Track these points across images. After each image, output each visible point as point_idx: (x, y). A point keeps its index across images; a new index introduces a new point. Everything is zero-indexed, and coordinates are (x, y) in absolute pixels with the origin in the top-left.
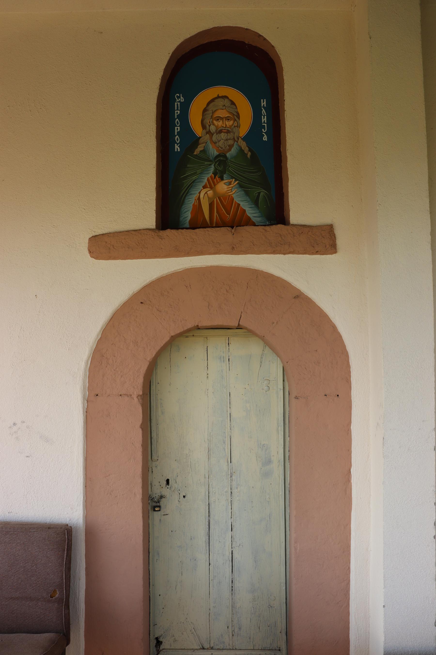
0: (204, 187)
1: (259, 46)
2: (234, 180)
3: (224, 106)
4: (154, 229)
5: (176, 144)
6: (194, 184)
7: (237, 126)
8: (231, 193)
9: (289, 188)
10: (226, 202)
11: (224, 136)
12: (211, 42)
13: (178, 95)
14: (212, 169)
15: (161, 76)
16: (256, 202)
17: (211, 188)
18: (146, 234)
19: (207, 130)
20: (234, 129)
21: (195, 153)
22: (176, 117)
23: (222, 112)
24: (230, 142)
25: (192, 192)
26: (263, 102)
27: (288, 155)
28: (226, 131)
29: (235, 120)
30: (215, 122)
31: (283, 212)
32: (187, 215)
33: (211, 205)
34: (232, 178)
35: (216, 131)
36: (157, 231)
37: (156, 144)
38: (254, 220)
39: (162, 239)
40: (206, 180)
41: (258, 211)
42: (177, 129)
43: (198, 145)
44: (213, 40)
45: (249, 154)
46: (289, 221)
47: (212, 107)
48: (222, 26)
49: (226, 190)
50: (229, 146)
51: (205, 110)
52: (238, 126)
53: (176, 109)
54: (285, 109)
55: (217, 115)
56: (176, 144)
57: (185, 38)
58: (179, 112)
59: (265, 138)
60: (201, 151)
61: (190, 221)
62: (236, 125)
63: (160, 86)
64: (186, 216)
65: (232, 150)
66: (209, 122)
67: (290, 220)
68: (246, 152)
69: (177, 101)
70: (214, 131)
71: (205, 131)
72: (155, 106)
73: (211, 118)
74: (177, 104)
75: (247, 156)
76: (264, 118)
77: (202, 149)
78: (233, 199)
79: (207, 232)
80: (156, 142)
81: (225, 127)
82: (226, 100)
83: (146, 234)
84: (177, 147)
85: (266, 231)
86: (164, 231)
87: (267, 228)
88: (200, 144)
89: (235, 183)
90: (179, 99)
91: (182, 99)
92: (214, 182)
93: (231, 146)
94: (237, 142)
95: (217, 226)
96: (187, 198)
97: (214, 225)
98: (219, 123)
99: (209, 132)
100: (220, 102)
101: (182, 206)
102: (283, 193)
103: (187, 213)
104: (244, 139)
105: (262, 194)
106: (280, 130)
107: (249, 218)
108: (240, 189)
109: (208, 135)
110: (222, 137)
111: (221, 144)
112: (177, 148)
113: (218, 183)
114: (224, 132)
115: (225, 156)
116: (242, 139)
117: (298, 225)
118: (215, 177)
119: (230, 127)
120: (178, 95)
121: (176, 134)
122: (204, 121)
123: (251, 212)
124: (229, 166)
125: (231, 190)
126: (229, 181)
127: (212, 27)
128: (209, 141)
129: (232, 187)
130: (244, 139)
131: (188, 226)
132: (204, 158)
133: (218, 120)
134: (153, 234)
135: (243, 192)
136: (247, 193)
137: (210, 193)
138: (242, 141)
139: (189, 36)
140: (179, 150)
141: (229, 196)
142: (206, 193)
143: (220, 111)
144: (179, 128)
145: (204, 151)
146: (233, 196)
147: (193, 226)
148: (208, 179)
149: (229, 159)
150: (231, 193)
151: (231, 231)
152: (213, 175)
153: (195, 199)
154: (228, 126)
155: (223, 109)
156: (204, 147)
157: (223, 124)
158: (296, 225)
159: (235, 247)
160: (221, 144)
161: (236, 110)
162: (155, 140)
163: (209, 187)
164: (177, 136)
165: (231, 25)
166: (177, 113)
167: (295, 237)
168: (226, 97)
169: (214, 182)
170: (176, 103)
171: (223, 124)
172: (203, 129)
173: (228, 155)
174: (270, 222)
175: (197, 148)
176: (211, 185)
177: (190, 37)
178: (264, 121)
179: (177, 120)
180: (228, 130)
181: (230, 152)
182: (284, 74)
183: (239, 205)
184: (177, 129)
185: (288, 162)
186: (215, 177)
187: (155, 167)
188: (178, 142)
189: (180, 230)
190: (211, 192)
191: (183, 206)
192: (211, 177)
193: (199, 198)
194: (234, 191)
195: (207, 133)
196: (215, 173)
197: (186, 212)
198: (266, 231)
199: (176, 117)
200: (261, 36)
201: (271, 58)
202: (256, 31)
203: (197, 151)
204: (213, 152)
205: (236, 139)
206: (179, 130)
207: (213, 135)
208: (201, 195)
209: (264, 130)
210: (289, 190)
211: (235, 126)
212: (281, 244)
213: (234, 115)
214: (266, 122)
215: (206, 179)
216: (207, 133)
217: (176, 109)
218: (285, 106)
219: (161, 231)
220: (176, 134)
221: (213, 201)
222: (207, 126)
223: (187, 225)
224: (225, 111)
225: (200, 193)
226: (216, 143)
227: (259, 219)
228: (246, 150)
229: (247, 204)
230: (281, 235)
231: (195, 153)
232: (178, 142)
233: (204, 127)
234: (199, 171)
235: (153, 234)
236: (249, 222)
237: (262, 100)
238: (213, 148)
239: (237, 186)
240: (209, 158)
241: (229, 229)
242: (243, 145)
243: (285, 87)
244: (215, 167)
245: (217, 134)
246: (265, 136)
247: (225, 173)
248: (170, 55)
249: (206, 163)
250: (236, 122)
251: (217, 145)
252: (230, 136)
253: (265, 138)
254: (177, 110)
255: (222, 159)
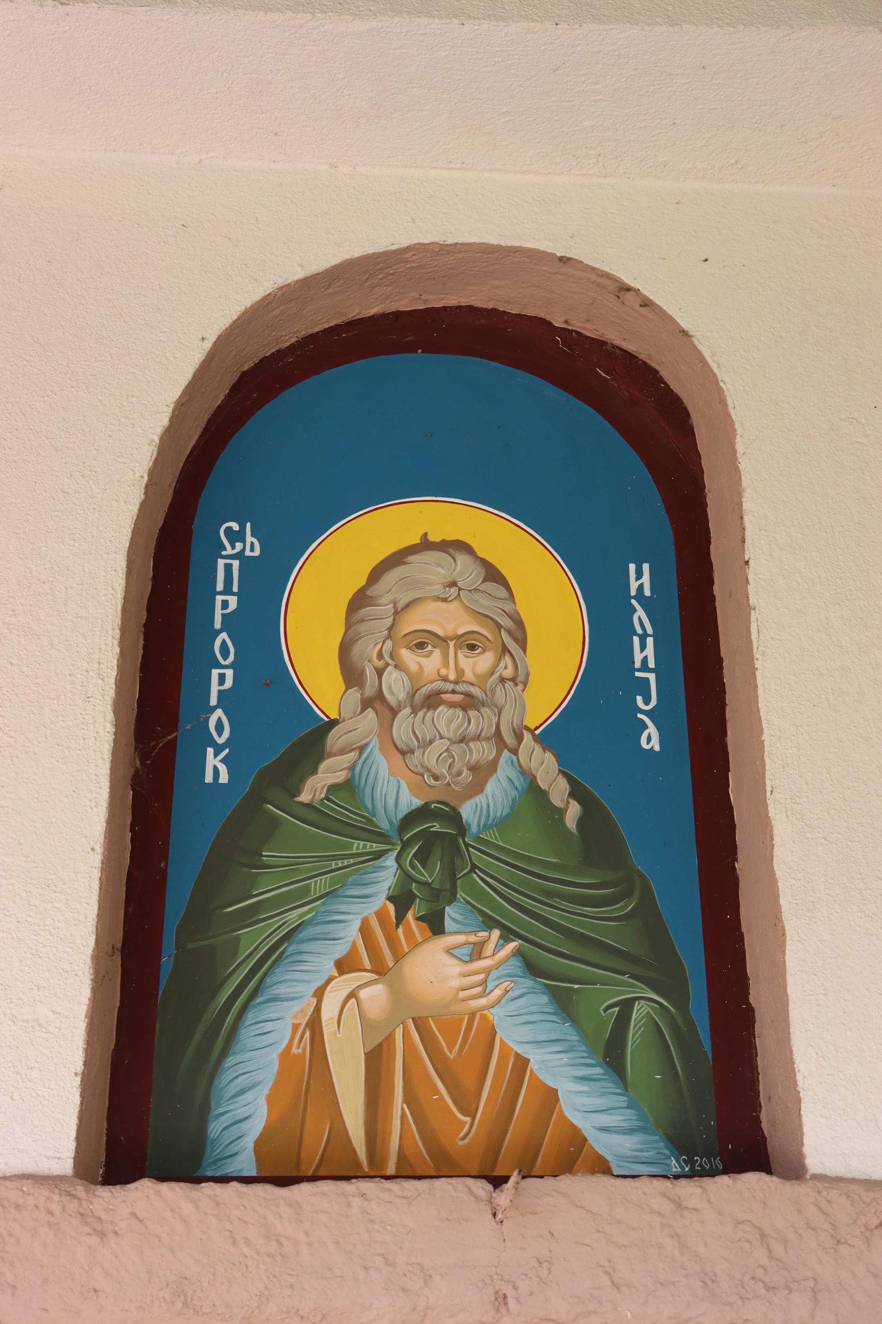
0: (344, 966)
1: (614, 336)
2: (496, 933)
3: (454, 584)
4: (61, 1178)
5: (210, 751)
6: (293, 948)
7: (513, 680)
8: (483, 1001)
9: (790, 980)
10: (455, 1046)
11: (450, 721)
12: (398, 314)
13: (235, 526)
14: (387, 874)
15: (159, 431)
16: (612, 1055)
17: (380, 970)
18: (18, 1207)
19: (370, 690)
20: (499, 693)
21: (305, 797)
22: (218, 625)
23: (432, 625)
24: (481, 752)
25: (282, 990)
26: (639, 574)
27: (775, 812)
28: (458, 698)
29: (505, 650)
30: (407, 656)
31: (756, 1107)
32: (246, 1106)
33: (376, 1061)
34: (490, 923)
35: (412, 696)
36: (80, 1190)
37: (111, 738)
38: (603, 1145)
39: (102, 1235)
40: (352, 932)
41: (622, 1101)
42: (222, 679)
43: (321, 757)
44: (405, 304)
45: (574, 810)
46: (801, 1156)
47: (390, 588)
48: (450, 241)
49: (456, 983)
50: (473, 769)
51: (360, 601)
52: (521, 679)
53: (220, 587)
54: (752, 602)
55: (413, 623)
56: (210, 751)
57: (281, 282)
58: (233, 601)
59: (651, 738)
60: (333, 788)
61: (259, 1144)
62: (509, 673)
63: (152, 473)
64: (242, 1112)
65: (491, 786)
66: (380, 656)
67: (806, 1150)
68: (557, 800)
69: (229, 551)
70: (402, 696)
71: (354, 695)
72: (121, 562)
73: (389, 637)
74: (228, 568)
75: (563, 824)
76: (643, 647)
77: (339, 777)
78: (494, 1033)
79: (356, 1202)
80: (111, 728)
81: (456, 683)
82: (463, 559)
83: (18, 1207)
84: (212, 760)
85: (679, 1205)
86: (118, 1190)
87: (688, 1189)
88: (331, 755)
89: (500, 952)
90: (234, 548)
91: (252, 546)
92: (393, 943)
93: (482, 773)
94: (515, 752)
95: (407, 1172)
96: (251, 1016)
97: (391, 1170)
98: (423, 661)
99: (374, 700)
100: (432, 569)
101: (224, 1053)
102: (750, 1010)
103: (249, 1096)
104: (550, 737)
105: (639, 1011)
106: (723, 705)
107: (578, 1140)
108: (529, 983)
109: (370, 713)
110: (442, 726)
111: (432, 757)
112: (215, 767)
113: (415, 945)
114: (451, 705)
115: (454, 818)
116: (536, 738)
117: (853, 1181)
118: (400, 917)
119: (482, 679)
120: (235, 526)
121: (213, 701)
122: (356, 651)
123: (589, 1105)
124: (474, 867)
125: (485, 981)
126: (472, 938)
127: (405, 243)
128: (375, 743)
129: (488, 971)
130: (550, 737)
131: (251, 1171)
132: (347, 820)
133: (421, 646)
134: (56, 1208)
135: (545, 999)
136: (565, 1004)
137: (375, 995)
138: (538, 749)
139: (299, 274)
140: (224, 778)
141: (472, 1016)
142: (352, 995)
143: (433, 605)
144: (229, 673)
145: (348, 788)
146: (496, 1015)
147: (281, 1170)
148: (365, 930)
149: (474, 829)
150: (483, 1001)
151: (490, 1201)
152: (391, 908)
153: (295, 1027)
154: (469, 676)
155: (445, 600)
156: (352, 768)
157: (446, 664)
158: (839, 1179)
159: (510, 1293)
160: (432, 757)
161: (508, 607)
162: (110, 716)
163: (367, 964)
164: (219, 713)
165: (494, 241)
166: (225, 604)
167: (844, 1249)
168: (462, 546)
169: (393, 943)
170: (221, 563)
171: (446, 664)
172: (348, 686)
173: (468, 811)
174: (690, 1162)
175: (314, 771)
176: (376, 958)
177: (306, 280)
178: (645, 660)
179: (224, 636)
180: (468, 695)
181: (479, 799)
182: (740, 448)
183: (522, 1063)
184: (222, 679)
185: (776, 851)
186: (400, 917)
187: (99, 849)
188: (221, 740)
189: (208, 1188)
190: (379, 989)
191: (230, 1061)
192: (381, 915)
193: (315, 1023)
194: (497, 993)
195: (366, 704)
196: (402, 900)
197: (243, 1091)
198: (679, 1205)
199: (218, 625)
200: (629, 289)
201: (668, 390)
202: (605, 268)
203: (313, 789)
204: (394, 793)
205: (509, 739)
206: (229, 683)
207: (394, 713)
208: (337, 997)
209: (647, 701)
210: (793, 990)
211: (502, 680)
212: (768, 1288)
213: (499, 626)
214: (652, 664)
215: (357, 924)
216: (366, 704)
217: (220, 587)
218: (751, 589)
219: (104, 1192)
220: (213, 701)
221: (390, 1038)
222: (369, 672)
223: (246, 1164)
224: (454, 606)
225: (319, 994)
226: (412, 752)
227: (628, 1144)
228: (559, 791)
229: (565, 1058)
230: (763, 1235)
231: (305, 797)
232: (221, 740)
233: (351, 675)
234: (319, 886)
235: (56, 1208)
236: (574, 1157)
237: (632, 567)
238: (392, 773)
239: (515, 965)
240: (370, 822)
241: (482, 1188)
242: (545, 767)
243: (747, 505)
244: (400, 866)
245: (414, 711)
246: (652, 729)
247: (453, 898)
248: (208, 345)
249: (358, 846)
250: (508, 659)
251: (415, 759)
252: (481, 721)
253: (651, 738)
254: (227, 591)
255: (436, 827)
